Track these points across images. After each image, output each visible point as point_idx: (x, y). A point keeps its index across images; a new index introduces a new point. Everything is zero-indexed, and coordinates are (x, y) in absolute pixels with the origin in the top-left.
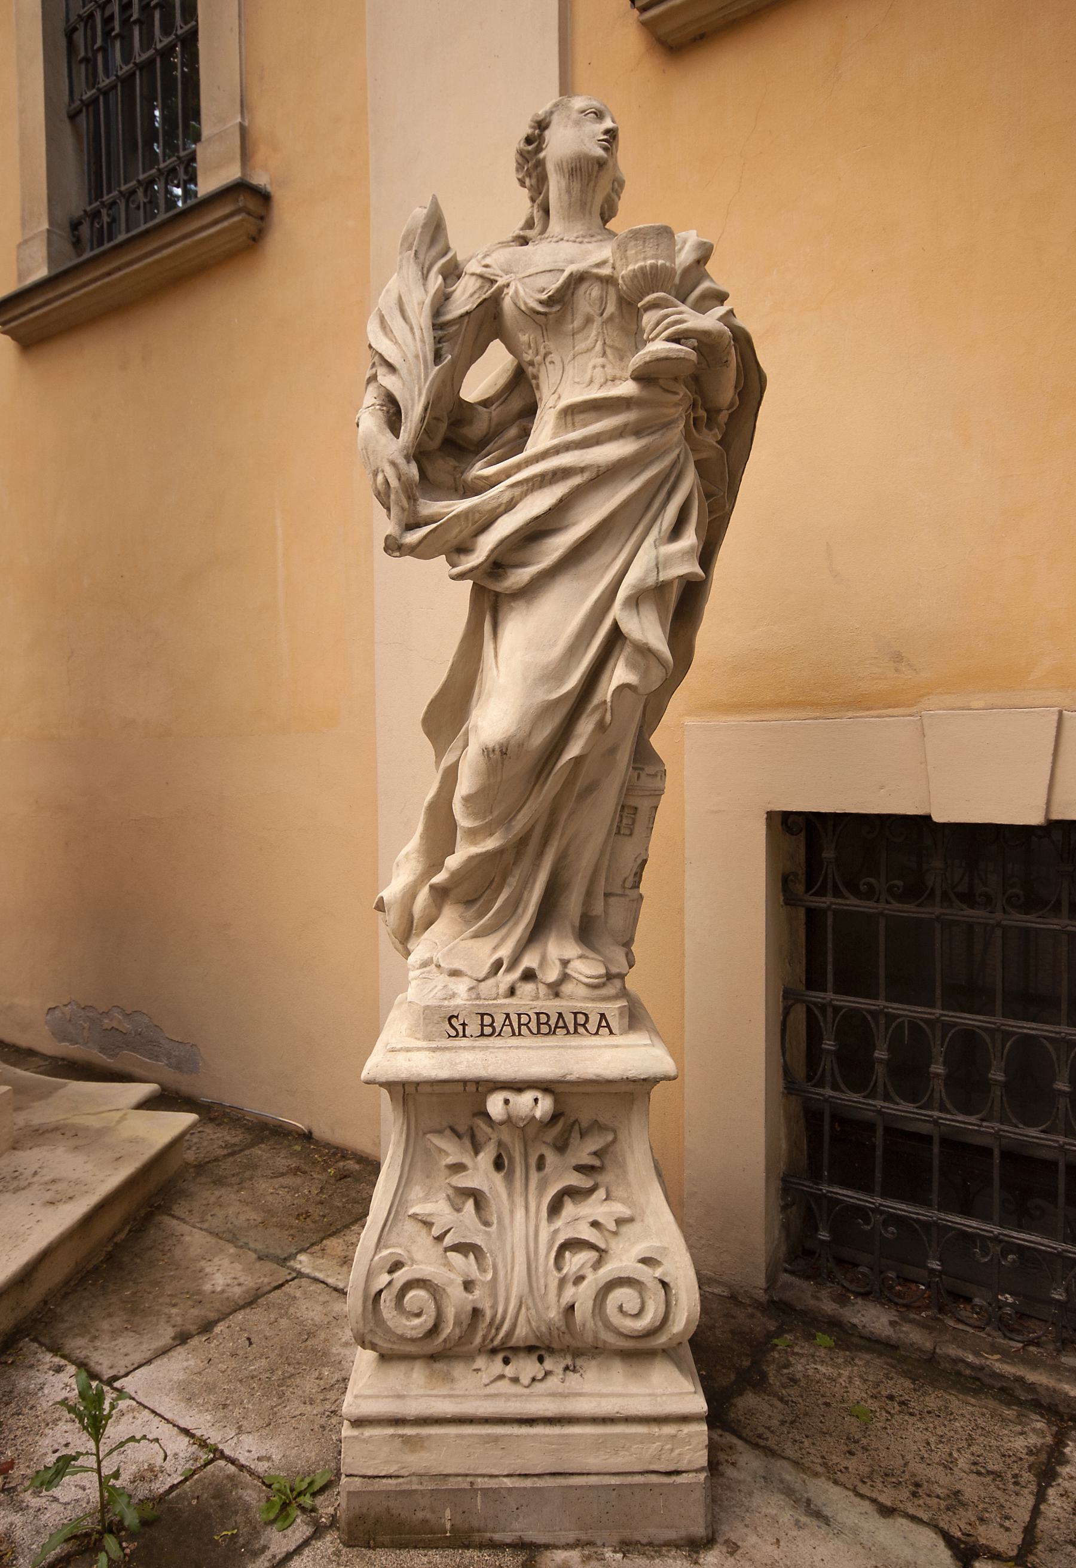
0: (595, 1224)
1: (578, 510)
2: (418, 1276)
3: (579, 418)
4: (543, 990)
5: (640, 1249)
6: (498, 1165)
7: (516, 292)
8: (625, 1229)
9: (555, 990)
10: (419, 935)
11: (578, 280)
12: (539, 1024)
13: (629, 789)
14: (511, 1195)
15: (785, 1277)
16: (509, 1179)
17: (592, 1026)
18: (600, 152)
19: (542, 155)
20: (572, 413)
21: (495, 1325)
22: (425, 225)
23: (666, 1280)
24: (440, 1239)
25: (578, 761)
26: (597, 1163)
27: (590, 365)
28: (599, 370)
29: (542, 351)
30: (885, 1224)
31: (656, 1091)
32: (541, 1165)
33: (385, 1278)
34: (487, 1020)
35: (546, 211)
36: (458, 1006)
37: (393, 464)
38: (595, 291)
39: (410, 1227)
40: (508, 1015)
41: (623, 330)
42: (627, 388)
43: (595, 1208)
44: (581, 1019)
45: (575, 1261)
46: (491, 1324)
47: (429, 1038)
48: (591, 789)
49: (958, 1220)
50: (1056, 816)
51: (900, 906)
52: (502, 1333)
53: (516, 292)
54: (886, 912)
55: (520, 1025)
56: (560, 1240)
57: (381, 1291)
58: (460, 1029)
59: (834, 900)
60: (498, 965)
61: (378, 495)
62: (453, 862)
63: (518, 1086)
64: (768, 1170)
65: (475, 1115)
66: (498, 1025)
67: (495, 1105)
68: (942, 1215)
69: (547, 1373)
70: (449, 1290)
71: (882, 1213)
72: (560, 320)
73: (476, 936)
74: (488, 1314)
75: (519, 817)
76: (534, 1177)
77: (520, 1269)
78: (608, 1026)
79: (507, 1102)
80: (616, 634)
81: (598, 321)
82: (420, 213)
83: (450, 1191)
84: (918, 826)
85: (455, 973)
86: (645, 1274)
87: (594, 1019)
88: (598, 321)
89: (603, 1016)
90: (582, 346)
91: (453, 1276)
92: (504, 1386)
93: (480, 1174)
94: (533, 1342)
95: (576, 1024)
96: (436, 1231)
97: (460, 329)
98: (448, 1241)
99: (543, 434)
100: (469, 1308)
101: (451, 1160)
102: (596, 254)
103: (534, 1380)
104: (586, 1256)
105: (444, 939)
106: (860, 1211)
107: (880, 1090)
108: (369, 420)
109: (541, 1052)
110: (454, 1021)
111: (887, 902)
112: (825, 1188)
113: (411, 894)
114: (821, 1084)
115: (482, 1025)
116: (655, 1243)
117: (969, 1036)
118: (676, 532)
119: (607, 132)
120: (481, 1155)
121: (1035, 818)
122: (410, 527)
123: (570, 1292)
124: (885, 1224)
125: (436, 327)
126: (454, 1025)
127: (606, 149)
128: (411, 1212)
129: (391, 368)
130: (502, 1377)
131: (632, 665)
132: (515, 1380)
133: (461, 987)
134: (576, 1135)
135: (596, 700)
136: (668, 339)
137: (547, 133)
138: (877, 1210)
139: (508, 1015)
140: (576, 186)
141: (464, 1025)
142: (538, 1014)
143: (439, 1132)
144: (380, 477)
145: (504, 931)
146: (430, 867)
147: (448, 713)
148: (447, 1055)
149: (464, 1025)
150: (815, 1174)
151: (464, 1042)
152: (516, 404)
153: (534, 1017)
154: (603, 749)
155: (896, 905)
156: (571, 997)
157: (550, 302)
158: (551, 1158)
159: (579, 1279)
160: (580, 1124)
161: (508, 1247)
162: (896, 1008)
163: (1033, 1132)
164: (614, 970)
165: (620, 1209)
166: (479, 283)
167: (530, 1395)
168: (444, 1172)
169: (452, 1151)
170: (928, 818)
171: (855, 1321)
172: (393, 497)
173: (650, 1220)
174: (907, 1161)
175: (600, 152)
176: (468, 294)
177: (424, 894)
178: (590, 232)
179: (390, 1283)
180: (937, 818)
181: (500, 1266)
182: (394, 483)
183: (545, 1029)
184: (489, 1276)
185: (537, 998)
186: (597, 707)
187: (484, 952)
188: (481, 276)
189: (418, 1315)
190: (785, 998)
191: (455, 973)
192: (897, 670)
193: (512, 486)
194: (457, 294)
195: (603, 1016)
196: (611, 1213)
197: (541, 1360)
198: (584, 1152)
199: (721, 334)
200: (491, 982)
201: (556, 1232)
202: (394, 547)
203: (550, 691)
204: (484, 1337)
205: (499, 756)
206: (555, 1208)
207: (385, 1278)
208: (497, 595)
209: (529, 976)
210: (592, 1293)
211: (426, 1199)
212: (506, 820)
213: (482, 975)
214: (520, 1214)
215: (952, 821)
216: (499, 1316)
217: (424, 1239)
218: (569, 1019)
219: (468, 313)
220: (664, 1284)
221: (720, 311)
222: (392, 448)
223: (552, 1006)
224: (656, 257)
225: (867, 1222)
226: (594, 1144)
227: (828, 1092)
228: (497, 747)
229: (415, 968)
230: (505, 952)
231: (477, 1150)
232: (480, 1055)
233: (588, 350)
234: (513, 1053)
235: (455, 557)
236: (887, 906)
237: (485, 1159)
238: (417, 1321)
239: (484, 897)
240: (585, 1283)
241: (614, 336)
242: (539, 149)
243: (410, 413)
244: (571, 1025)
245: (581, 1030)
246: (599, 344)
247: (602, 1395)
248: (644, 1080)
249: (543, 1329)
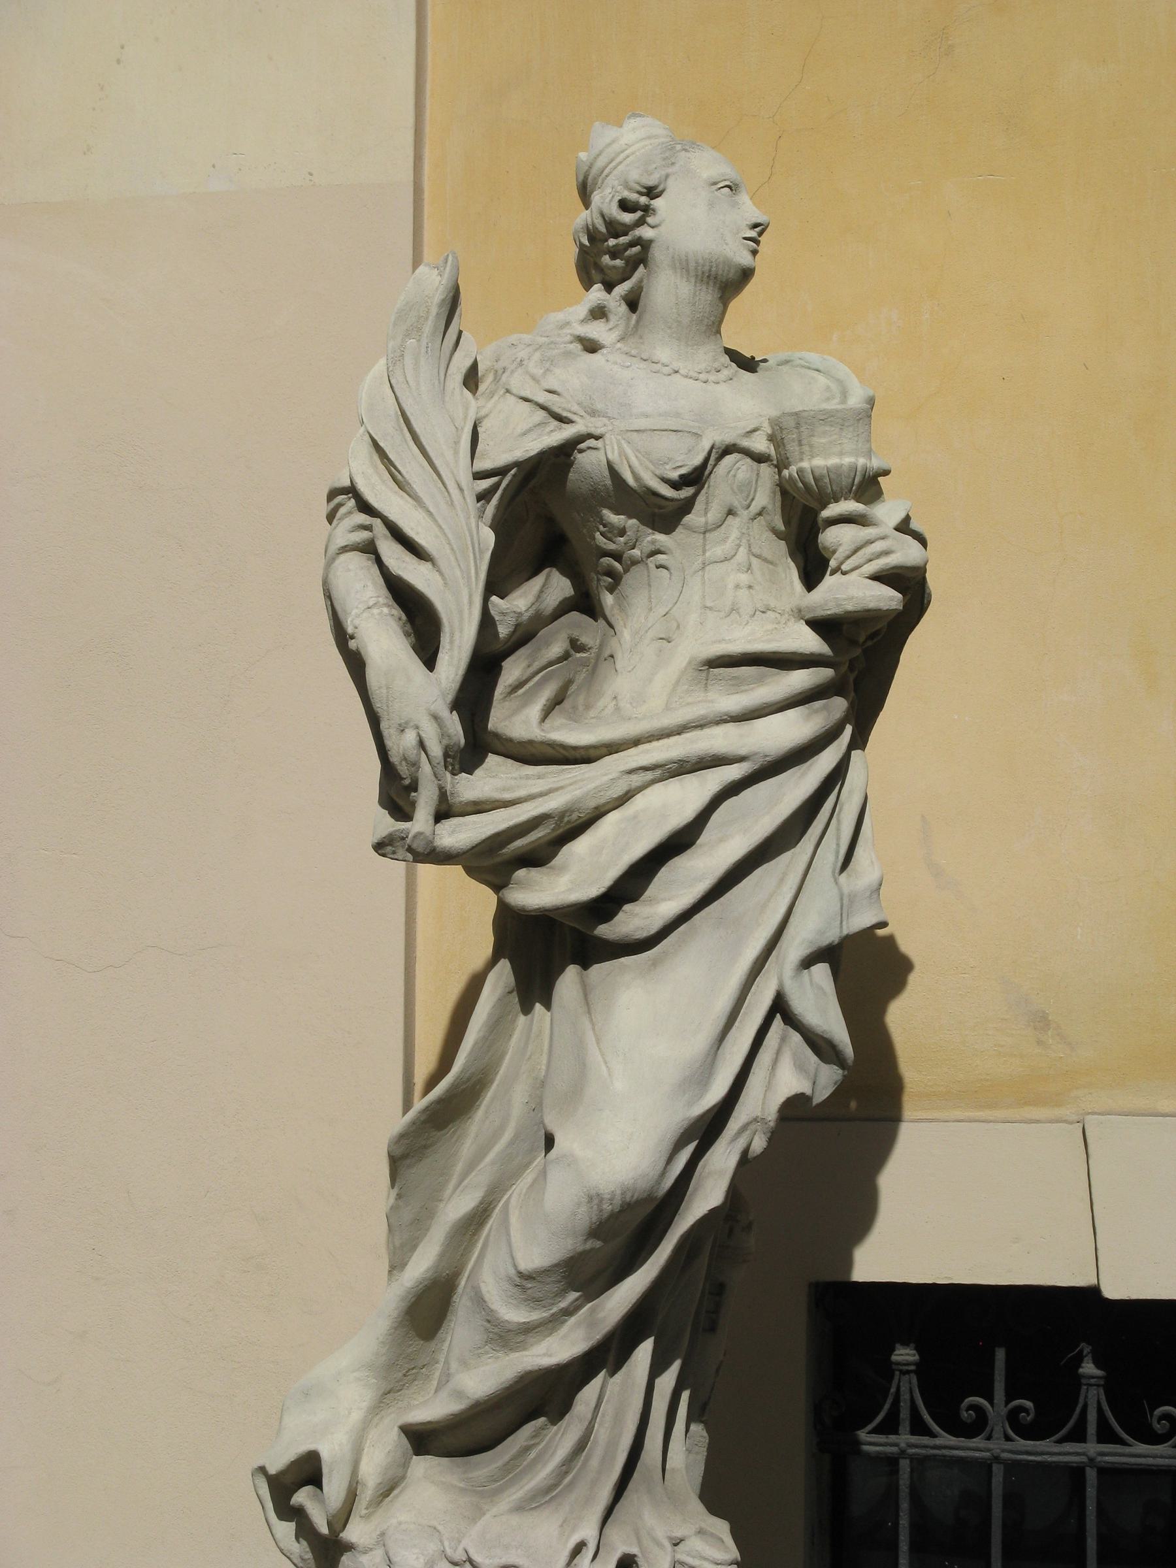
18: (745, 259)
28: (743, 593)
37: (436, 718)
51: (1030, 1444)
54: (1005, 1455)
59: (914, 1439)
73: (520, 1508)
80: (780, 1007)
90: (717, 551)
97: (495, 488)
111: (1008, 1439)
136: (877, 577)
155: (1021, 1443)
170: (1092, 1294)
178: (716, 365)
180: (1112, 1291)
192: (1039, 1043)
203: (690, 1104)
215: (1134, 1297)
228: (618, 1192)
236: (1008, 1445)
243: (457, 635)
246: (743, 551)
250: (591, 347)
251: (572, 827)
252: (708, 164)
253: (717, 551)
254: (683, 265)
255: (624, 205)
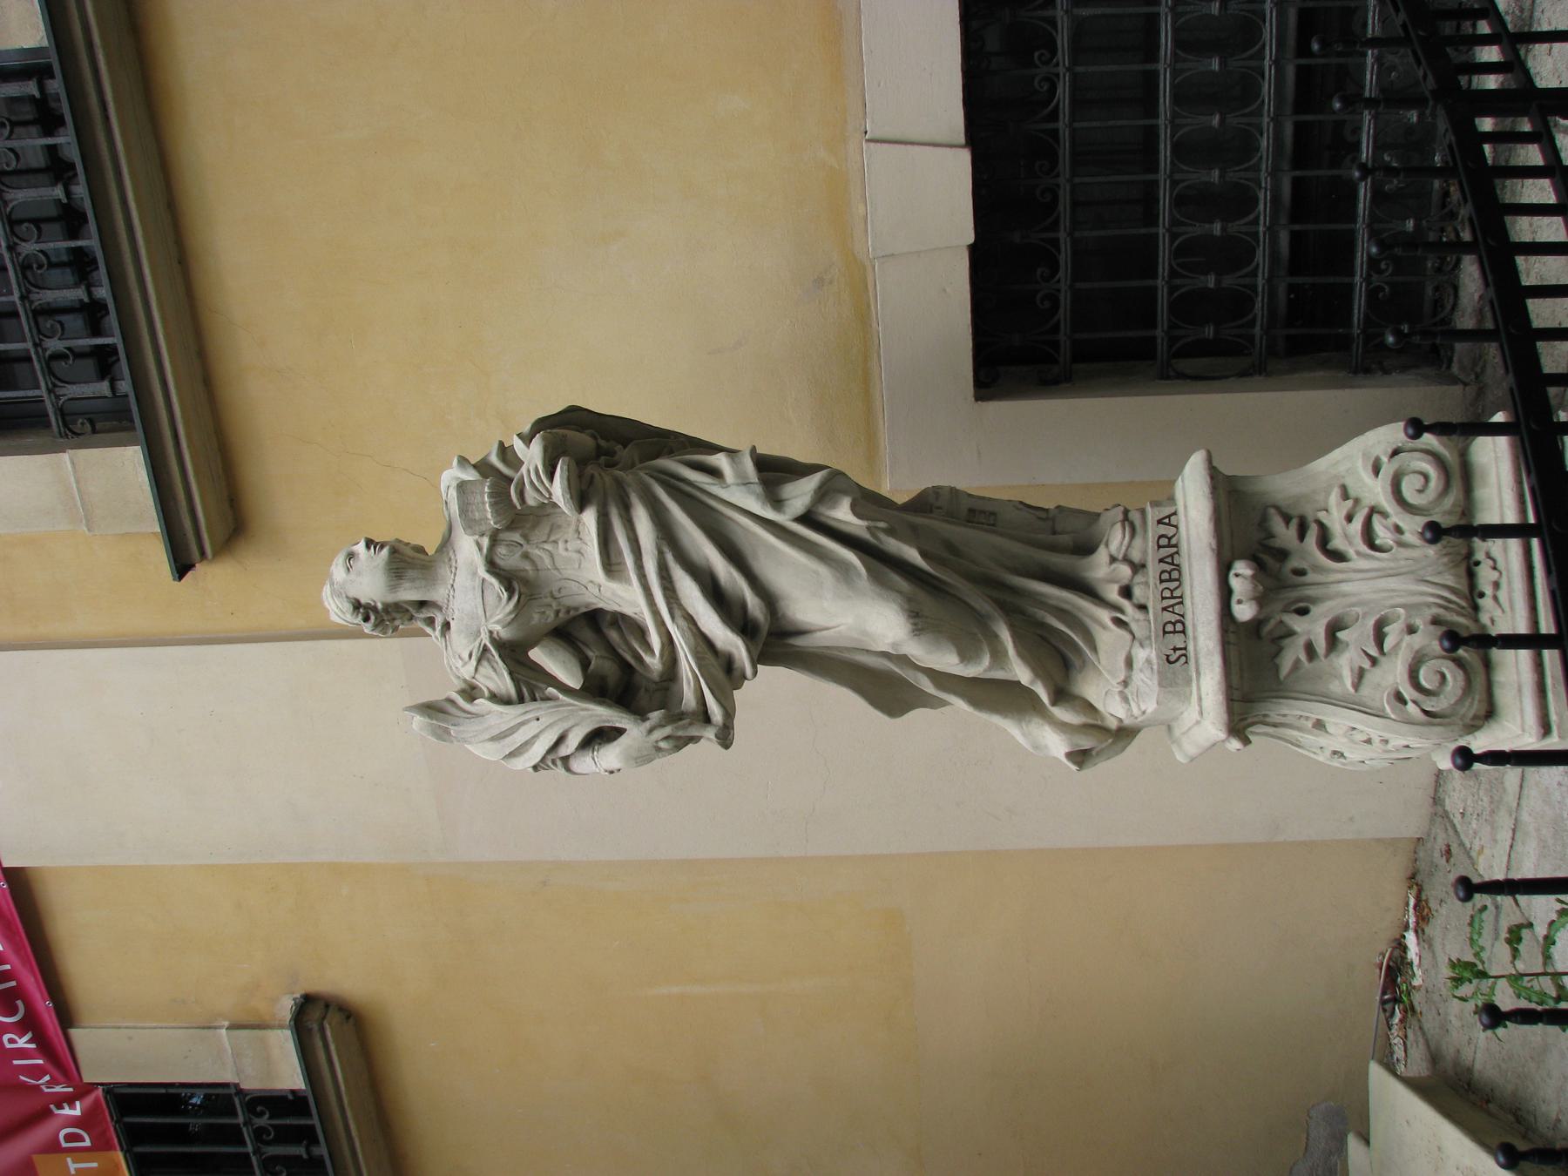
0: (1349, 518)
1: (695, 557)
2: (1406, 676)
3: (614, 559)
4: (1139, 578)
5: (1366, 476)
6: (1303, 612)
7: (498, 622)
8: (1352, 493)
9: (1138, 568)
10: (1103, 719)
11: (492, 566)
12: (1170, 580)
13: (951, 517)
14: (1329, 598)
15: (1455, 369)
16: (1314, 600)
17: (1170, 531)
18: (385, 551)
19: (380, 606)
20: (611, 565)
21: (1447, 605)
22: (430, 717)
23: (1390, 451)
24: (1374, 661)
25: (924, 554)
26: (1295, 522)
27: (564, 554)
29: (549, 600)
30: (1380, 272)
31: (1227, 469)
32: (1300, 573)
33: (1411, 707)
34: (1169, 628)
35: (422, 604)
36: (1158, 657)
37: (650, 731)
38: (502, 550)
39: (1365, 690)
40: (1164, 609)
41: (535, 525)
42: (590, 518)
43: (1334, 519)
44: (1164, 541)
45: (1383, 535)
46: (1446, 608)
47: (1189, 682)
48: (951, 547)
49: (1361, 206)
50: (962, 139)
52: (1453, 598)
53: (498, 622)
55: (1172, 597)
56: (1364, 549)
57: (1426, 712)
58: (1179, 653)
60: (1119, 623)
61: (678, 748)
62: (1021, 673)
63: (1225, 593)
64: (1343, 387)
65: (1259, 637)
66: (1174, 618)
67: (1244, 611)
68: (1360, 219)
69: (1488, 556)
70: (1416, 647)
71: (1369, 275)
72: (526, 582)
73: (1094, 649)
74: (1435, 610)
75: (977, 606)
76: (1311, 577)
77: (1392, 583)
78: (1169, 517)
79: (1239, 602)
80: (807, 519)
81: (526, 547)
82: (418, 720)
83: (1332, 656)
84: (977, 253)
85: (1129, 663)
86: (1388, 469)
87: (1163, 530)
88: (526, 547)
89: (1159, 522)
90: (547, 561)
91: (1404, 645)
92: (1502, 595)
93: (1313, 628)
94: (1462, 570)
95: (1169, 546)
96: (1366, 664)
98: (1374, 652)
99: (625, 597)
100: (1432, 628)
101: (1303, 657)
102: (468, 550)
103: (1495, 568)
104: (1377, 523)
105: (1102, 691)
106: (1372, 294)
107: (1247, 281)
108: (610, 756)
109: (1195, 574)
110: (1172, 659)
112: (1356, 331)
113: (1062, 727)
114: (1251, 339)
115: (1175, 632)
116: (1360, 463)
117: (1179, 201)
118: (715, 473)
119: (368, 547)
120: (1297, 628)
121: (965, 156)
122: (707, 719)
123: (1409, 537)
124: (1380, 272)
125: (521, 700)
126: (1176, 659)
127: (382, 547)
128: (1351, 690)
129: (561, 740)
130: (1495, 598)
131: (834, 506)
132: (1496, 585)
133: (1141, 655)
134: (1272, 543)
135: (866, 536)
136: (551, 477)
137: (363, 601)
138: (1368, 279)
139: (1164, 609)
140: (411, 573)
141: (1175, 649)
142: (1162, 581)
143: (1277, 668)
144: (663, 745)
145: (1088, 622)
146: (1034, 709)
147: (886, 687)
148: (1202, 660)
149: (1175, 649)
150: (1344, 344)
151: (1191, 648)
152: (586, 634)
153: (1165, 585)
154: (914, 535)
155: (1061, 274)
156: (1145, 552)
157: (510, 590)
158: (1294, 563)
159: (1398, 530)
160: (1258, 535)
161: (1374, 596)
162: (1163, 268)
163: (1264, 143)
164: (1121, 517)
165: (1334, 498)
166: (485, 663)
167: (1508, 571)
168: (1315, 664)
169: (1293, 653)
170: (973, 249)
171: (1476, 297)
172: (680, 733)
173: (1342, 469)
174: (1318, 254)
175: (385, 551)
176: (493, 674)
177: (1060, 713)
179: (1414, 702)
180: (971, 239)
181: (1392, 602)
182: (667, 730)
183: (1175, 575)
184: (1401, 610)
185: (1147, 584)
186: (873, 535)
187: (1109, 638)
188: (479, 661)
189: (1443, 676)
190: (1168, 378)
191: (1129, 663)
193: (673, 618)
194: (493, 687)
195: (1159, 522)
196: (1338, 505)
197: (1477, 563)
198: (1285, 535)
199: (544, 438)
200: (1134, 626)
201: (1358, 553)
202: (725, 737)
203: (859, 575)
204: (1459, 614)
205: (920, 622)
206: (1338, 556)
207: (1411, 707)
208: (770, 634)
209: (1127, 592)
210: (1408, 517)
211: (1339, 677)
212: (982, 621)
213: (1128, 636)
214: (1345, 587)
216: (1432, 600)
217: (1373, 676)
218: (1164, 552)
219: (511, 673)
220: (1395, 453)
221: (518, 445)
222: (635, 732)
223: (1153, 569)
224: (482, 493)
225: (1379, 289)
226: (1277, 525)
227: (1257, 330)
229: (1130, 710)
230: (1105, 615)
231: (1291, 633)
232: (1200, 629)
233: (552, 556)
234: (1197, 599)
235: (736, 674)
237: (1297, 624)
238: (1448, 676)
239: (1062, 648)
240: (1401, 524)
241: (540, 534)
242: (375, 609)
244: (1170, 549)
245: (1174, 541)
246: (547, 546)
247: (1501, 506)
248: (1212, 478)
249: (1445, 560)
250: (447, 626)
251: (704, 643)
252: (338, 571)
253: (547, 561)
254: (393, 588)
255: (366, 619)
